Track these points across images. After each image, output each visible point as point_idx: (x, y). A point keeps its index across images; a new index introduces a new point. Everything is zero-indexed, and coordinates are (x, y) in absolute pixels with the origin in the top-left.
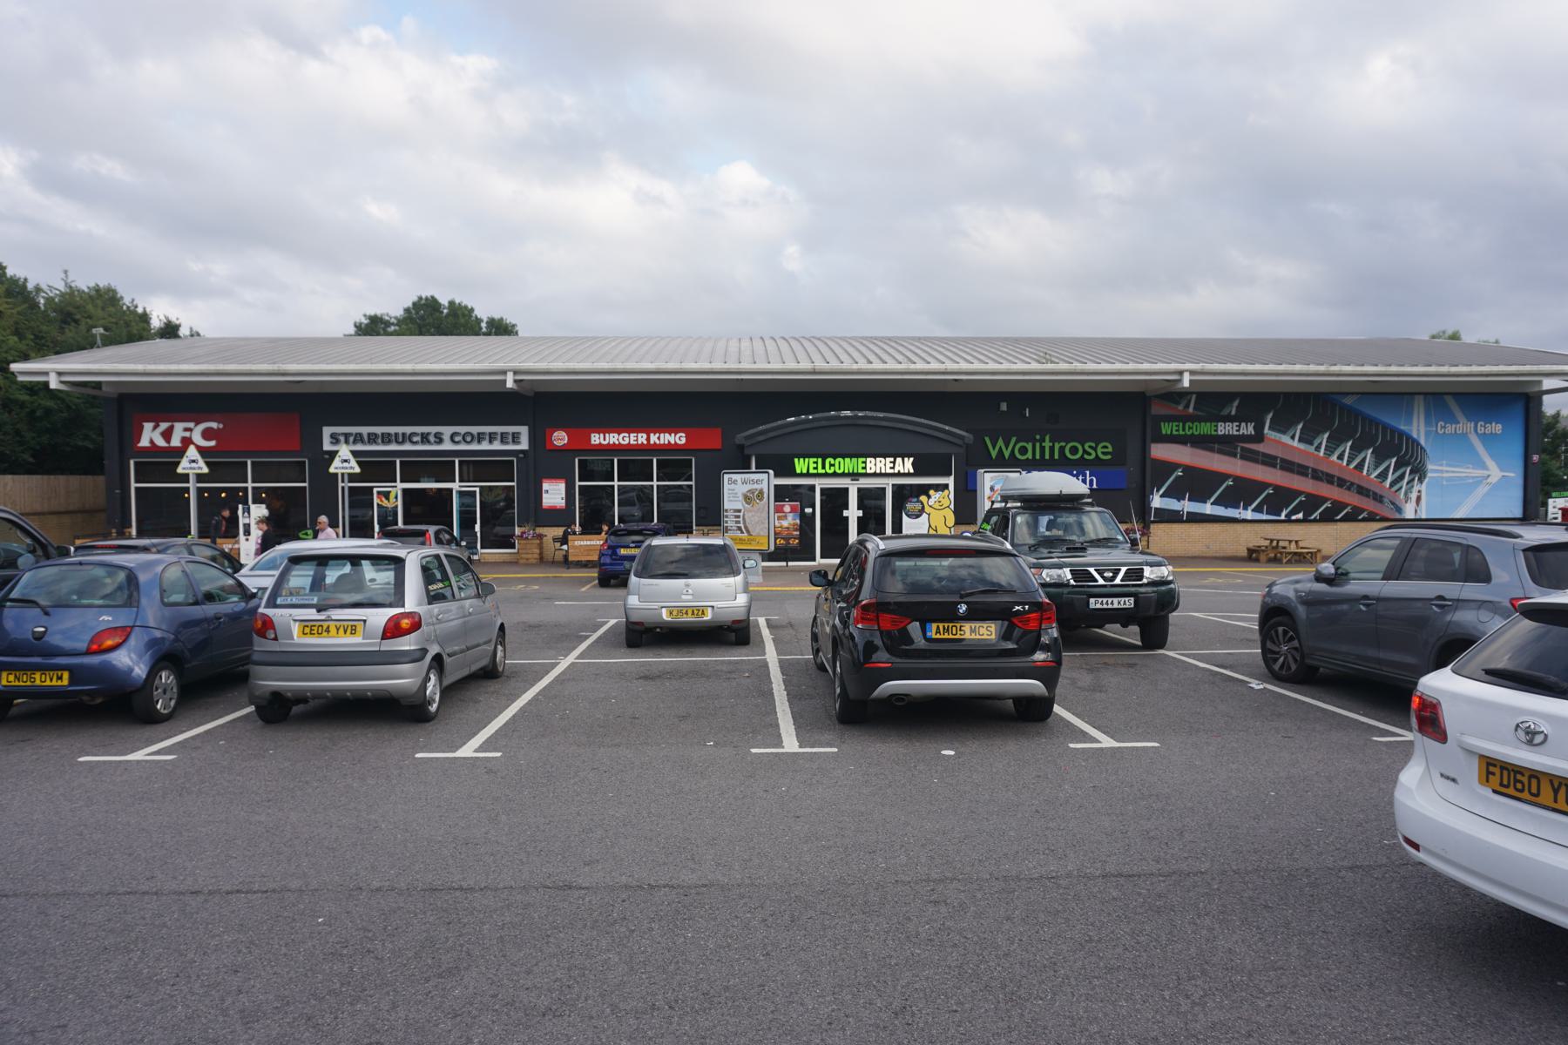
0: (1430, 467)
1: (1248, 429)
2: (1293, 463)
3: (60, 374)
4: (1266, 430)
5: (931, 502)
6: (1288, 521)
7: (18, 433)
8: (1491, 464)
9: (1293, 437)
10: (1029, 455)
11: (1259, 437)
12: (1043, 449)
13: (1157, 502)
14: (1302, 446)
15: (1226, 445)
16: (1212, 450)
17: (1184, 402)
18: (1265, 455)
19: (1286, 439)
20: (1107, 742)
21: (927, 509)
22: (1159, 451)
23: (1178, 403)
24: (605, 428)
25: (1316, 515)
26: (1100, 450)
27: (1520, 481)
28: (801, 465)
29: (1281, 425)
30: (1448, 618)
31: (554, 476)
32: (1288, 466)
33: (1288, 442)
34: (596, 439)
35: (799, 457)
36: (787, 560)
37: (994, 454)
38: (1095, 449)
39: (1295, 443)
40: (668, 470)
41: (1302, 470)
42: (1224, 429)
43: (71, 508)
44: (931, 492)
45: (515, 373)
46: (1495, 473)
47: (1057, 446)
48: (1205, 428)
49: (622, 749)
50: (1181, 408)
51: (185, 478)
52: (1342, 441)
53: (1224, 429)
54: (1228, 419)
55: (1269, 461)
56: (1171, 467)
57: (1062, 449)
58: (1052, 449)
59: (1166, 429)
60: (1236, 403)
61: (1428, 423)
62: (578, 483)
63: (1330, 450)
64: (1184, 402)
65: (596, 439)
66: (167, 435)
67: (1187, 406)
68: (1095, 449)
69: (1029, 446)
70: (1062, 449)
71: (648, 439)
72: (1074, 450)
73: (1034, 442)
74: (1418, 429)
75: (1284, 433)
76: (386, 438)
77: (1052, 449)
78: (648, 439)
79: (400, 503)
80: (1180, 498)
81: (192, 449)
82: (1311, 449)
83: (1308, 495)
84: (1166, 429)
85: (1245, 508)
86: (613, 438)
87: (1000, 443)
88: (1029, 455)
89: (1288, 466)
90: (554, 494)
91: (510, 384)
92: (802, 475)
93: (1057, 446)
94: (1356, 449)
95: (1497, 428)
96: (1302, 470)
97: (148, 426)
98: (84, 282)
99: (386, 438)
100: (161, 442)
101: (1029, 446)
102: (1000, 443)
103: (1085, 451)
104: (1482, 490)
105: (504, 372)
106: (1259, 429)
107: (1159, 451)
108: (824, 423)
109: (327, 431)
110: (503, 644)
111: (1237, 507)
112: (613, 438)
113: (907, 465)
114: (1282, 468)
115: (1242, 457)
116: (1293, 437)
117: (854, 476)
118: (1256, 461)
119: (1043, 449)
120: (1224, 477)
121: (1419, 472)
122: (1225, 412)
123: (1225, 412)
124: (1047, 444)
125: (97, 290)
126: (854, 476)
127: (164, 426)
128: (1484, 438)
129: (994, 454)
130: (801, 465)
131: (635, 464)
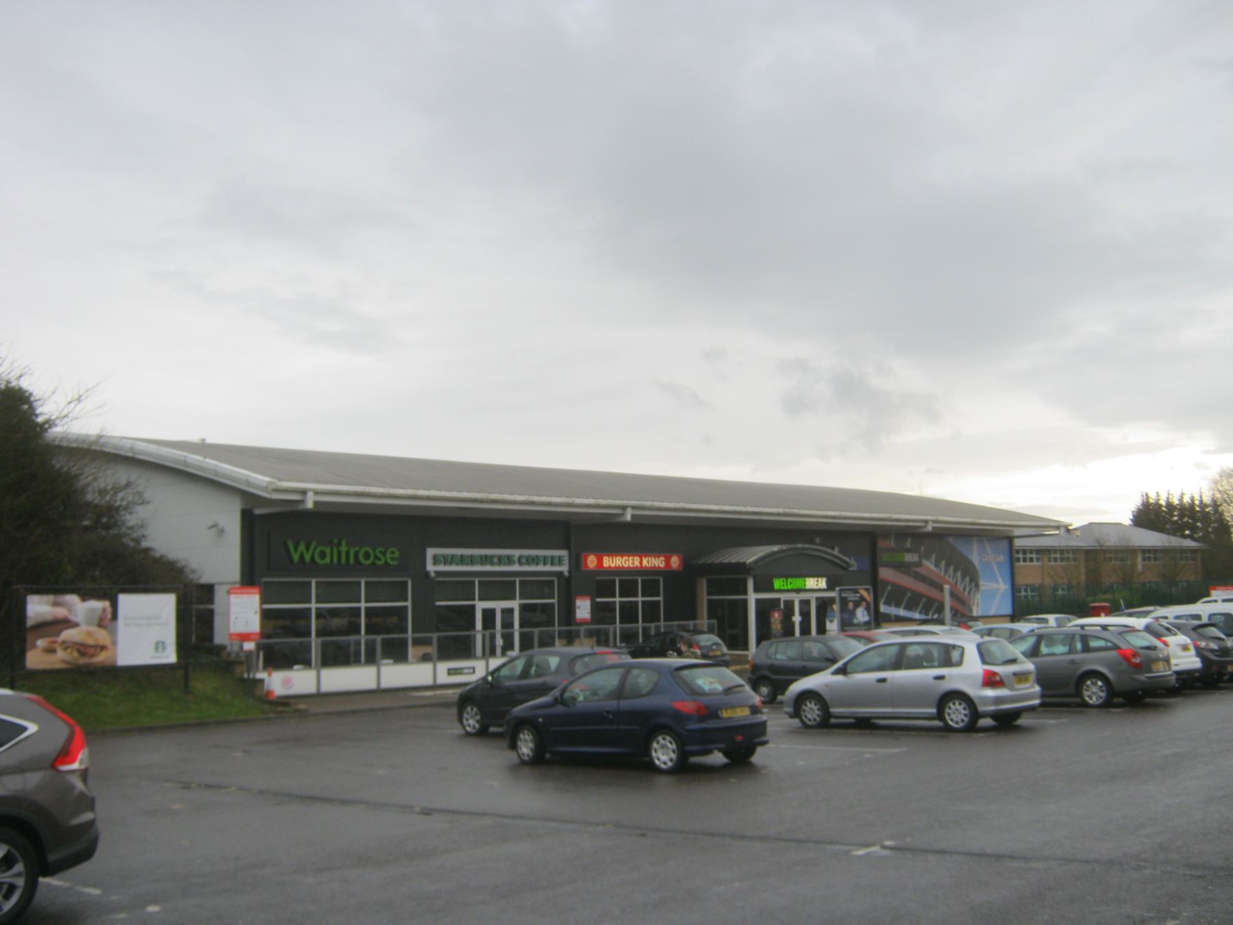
0: (981, 583)
12: (339, 553)
26: (388, 555)
28: (778, 583)
30: (261, 675)
37: (296, 557)
38: (384, 554)
40: (628, 588)
49: (398, 780)
57: (356, 555)
58: (348, 553)
63: (946, 571)
68: (384, 554)
69: (328, 550)
70: (356, 555)
71: (641, 562)
72: (367, 556)
73: (330, 543)
77: (348, 553)
78: (641, 562)
79: (675, 623)
87: (302, 547)
88: (328, 560)
90: (583, 609)
94: (955, 571)
101: (328, 550)
102: (302, 547)
108: (816, 553)
109: (431, 552)
113: (822, 583)
117: (798, 591)
119: (339, 553)
124: (344, 548)
126: (798, 591)
129: (296, 557)
130: (778, 583)
131: (628, 582)
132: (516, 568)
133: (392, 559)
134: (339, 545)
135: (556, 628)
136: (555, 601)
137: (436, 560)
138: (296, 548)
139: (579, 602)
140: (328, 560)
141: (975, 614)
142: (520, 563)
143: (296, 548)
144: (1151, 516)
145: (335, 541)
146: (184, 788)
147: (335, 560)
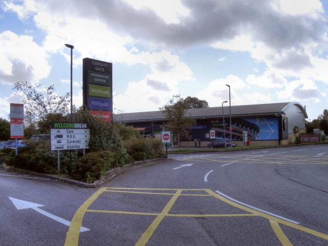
0: (260, 130)
6: (235, 140)
7: (36, 108)
8: (272, 130)
14: (237, 127)
20: (275, 221)
27: (278, 133)
46: (273, 131)
52: (244, 126)
59: (213, 125)
61: (259, 122)
63: (241, 128)
74: (257, 123)
81: (164, 137)
84: (213, 125)
95: (272, 123)
98: (184, 97)
104: (270, 134)
105: (275, 113)
110: (142, 150)
121: (258, 131)
128: (271, 125)
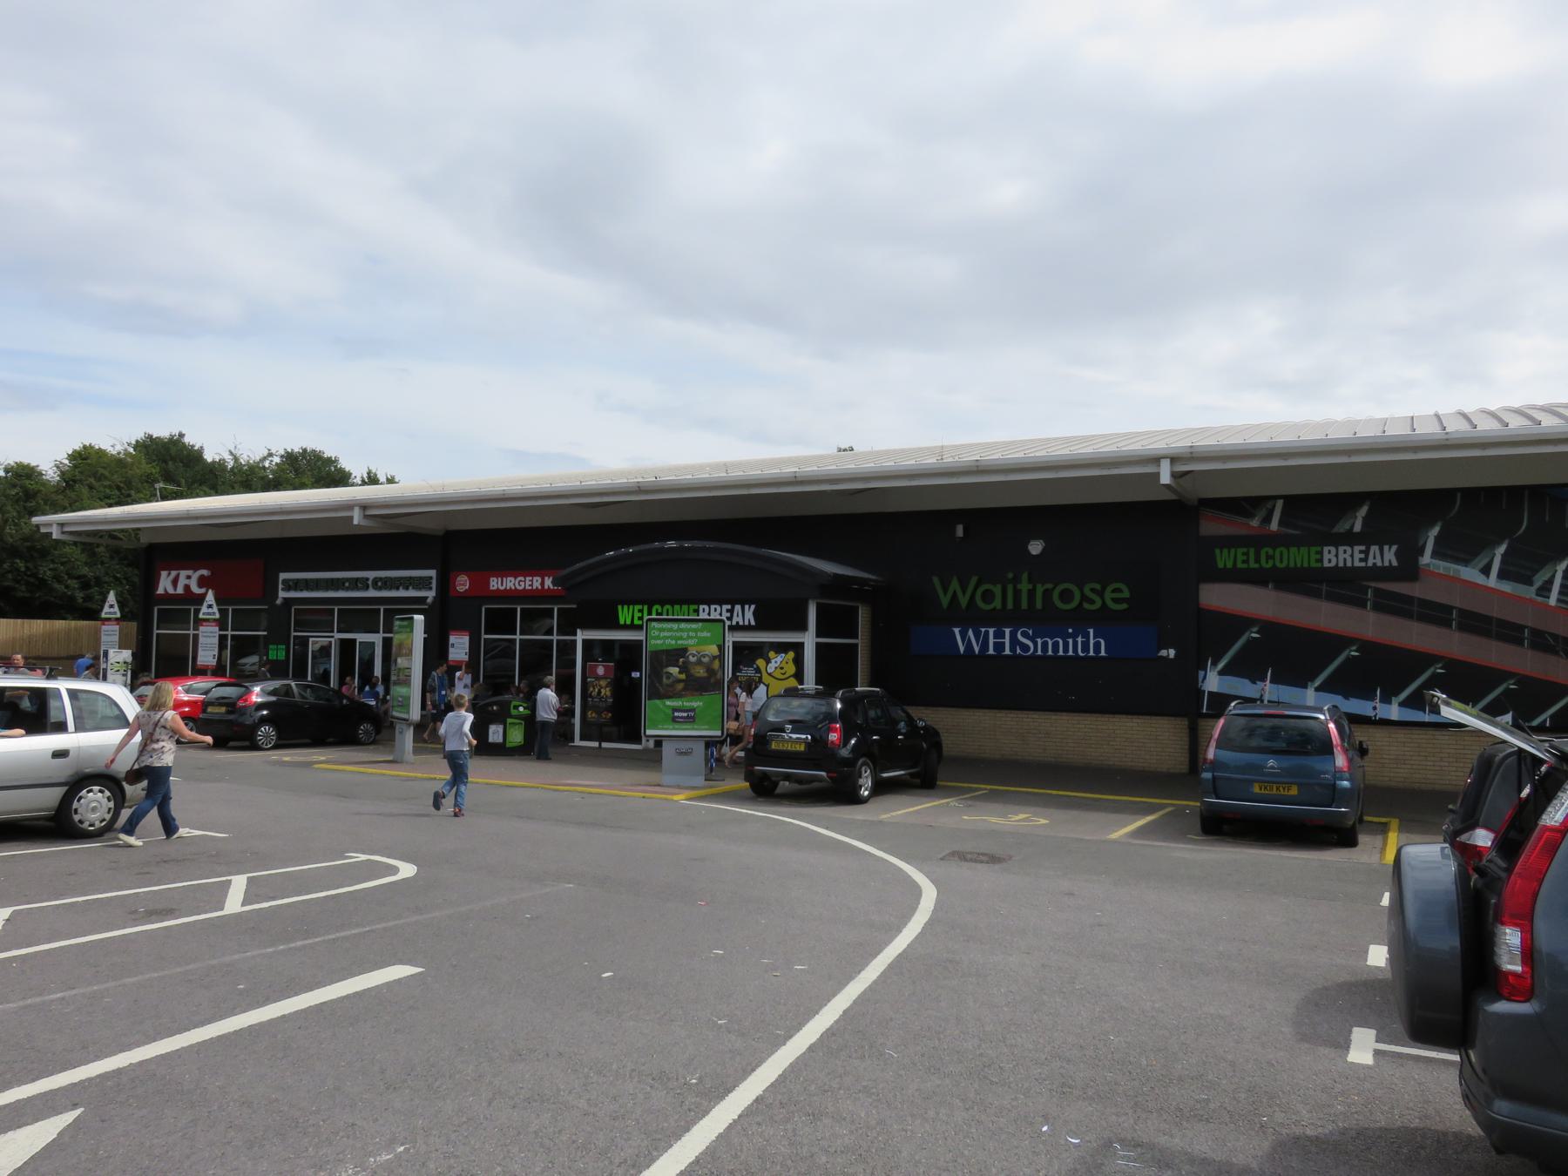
1: (1388, 556)
2: (1487, 619)
3: (62, 525)
4: (1426, 559)
5: (771, 667)
9: (1486, 571)
10: (997, 604)
11: (1408, 569)
12: (1017, 593)
13: (1213, 682)
14: (1507, 587)
15: (1345, 586)
16: (1316, 594)
17: (1263, 513)
18: (1424, 603)
19: (1470, 573)
21: (766, 678)
22: (1215, 596)
23: (1251, 516)
24: (504, 572)
25: (1545, 717)
26: (1108, 595)
28: (625, 615)
29: (1457, 547)
31: (459, 628)
32: (1475, 623)
33: (1482, 579)
34: (495, 584)
35: (623, 604)
36: (601, 739)
37: (945, 601)
38: (1101, 594)
39: (1492, 581)
41: (1509, 632)
42: (1333, 557)
43: (54, 653)
44: (772, 654)
45: (1174, 460)
47: (1040, 589)
48: (1297, 557)
50: (1255, 523)
51: (388, 629)
53: (1333, 557)
54: (1349, 539)
55: (1436, 614)
56: (1239, 623)
57: (1047, 594)
58: (1031, 593)
59: (1224, 559)
60: (1363, 511)
62: (484, 636)
64: (1263, 513)
65: (495, 584)
66: (175, 582)
67: (1267, 519)
68: (1101, 594)
69: (997, 590)
71: (542, 584)
75: (1466, 562)
76: (356, 584)
77: (1031, 593)
78: (542, 584)
80: (1256, 676)
82: (1529, 592)
83: (1524, 680)
84: (1224, 559)
85: (1386, 699)
86: (510, 583)
87: (955, 585)
89: (1475, 623)
91: (1165, 479)
92: (625, 627)
93: (1040, 589)
96: (1509, 632)
97: (164, 574)
99: (356, 584)
100: (171, 591)
102: (955, 585)
103: (1084, 598)
106: (1408, 554)
107: (1215, 596)
111: (1371, 697)
112: (510, 583)
113: (748, 615)
114: (1463, 628)
115: (1377, 608)
116: (1486, 571)
118: (1408, 615)
120: (1342, 642)
122: (1342, 527)
123: (1342, 527)
125: (85, 447)
127: (174, 573)
129: (945, 601)
130: (625, 615)
132: (372, 593)
133: (1115, 601)
134: (1016, 580)
135: (191, 632)
136: (484, 636)
137: (289, 586)
138: (945, 591)
139: (453, 639)
140: (997, 604)
141: (500, 740)
142: (376, 587)
143: (945, 591)
144: (138, 445)
145: (1010, 575)
146: (221, 744)
147: (1010, 605)
